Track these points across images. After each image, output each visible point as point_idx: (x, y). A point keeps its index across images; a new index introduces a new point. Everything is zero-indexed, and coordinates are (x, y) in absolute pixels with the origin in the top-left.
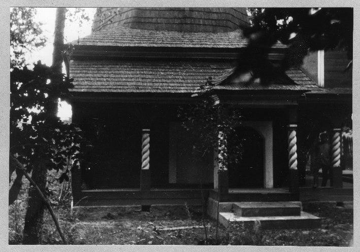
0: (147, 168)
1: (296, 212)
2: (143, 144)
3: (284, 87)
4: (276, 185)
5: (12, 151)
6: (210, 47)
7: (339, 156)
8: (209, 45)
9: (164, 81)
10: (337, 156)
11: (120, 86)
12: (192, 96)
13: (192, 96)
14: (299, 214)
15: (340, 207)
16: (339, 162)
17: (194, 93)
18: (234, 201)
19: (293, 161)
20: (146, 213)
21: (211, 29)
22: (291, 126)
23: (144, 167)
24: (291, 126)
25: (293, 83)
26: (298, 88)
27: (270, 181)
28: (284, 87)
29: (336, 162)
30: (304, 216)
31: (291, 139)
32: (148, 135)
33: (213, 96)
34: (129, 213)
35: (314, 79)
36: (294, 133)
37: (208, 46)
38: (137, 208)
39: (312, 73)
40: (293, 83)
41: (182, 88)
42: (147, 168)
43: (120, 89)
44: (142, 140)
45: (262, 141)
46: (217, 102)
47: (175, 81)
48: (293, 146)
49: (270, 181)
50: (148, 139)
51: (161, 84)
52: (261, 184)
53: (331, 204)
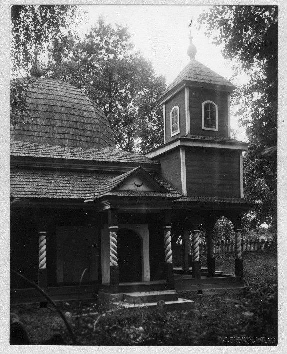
0: (45, 267)
1: (175, 297)
2: (41, 245)
3: (161, 195)
4: (152, 279)
5: (275, 302)
6: (91, 160)
7: (199, 253)
8: (91, 158)
9: (57, 188)
10: (197, 252)
11: (19, 191)
12: (85, 201)
13: (85, 201)
14: (177, 300)
15: (200, 294)
16: (199, 257)
17: (86, 199)
18: (125, 292)
19: (169, 256)
20: (45, 309)
21: (86, 144)
22: (167, 227)
23: (42, 266)
24: (167, 227)
25: (169, 192)
26: (172, 196)
27: (147, 275)
28: (161, 195)
29: (197, 257)
30: (181, 301)
31: (167, 238)
32: (45, 236)
33: (103, 202)
34: (29, 310)
35: (179, 189)
36: (169, 233)
37: (89, 159)
38: (35, 304)
39: (177, 184)
40: (169, 192)
41: (75, 195)
42: (45, 267)
43: (20, 194)
44: (39, 241)
45: (140, 241)
46: (108, 207)
47: (66, 188)
48: (169, 243)
49: (147, 275)
50: (45, 241)
51: (55, 191)
52: (140, 278)
53: (194, 292)
